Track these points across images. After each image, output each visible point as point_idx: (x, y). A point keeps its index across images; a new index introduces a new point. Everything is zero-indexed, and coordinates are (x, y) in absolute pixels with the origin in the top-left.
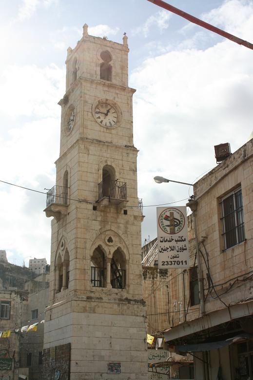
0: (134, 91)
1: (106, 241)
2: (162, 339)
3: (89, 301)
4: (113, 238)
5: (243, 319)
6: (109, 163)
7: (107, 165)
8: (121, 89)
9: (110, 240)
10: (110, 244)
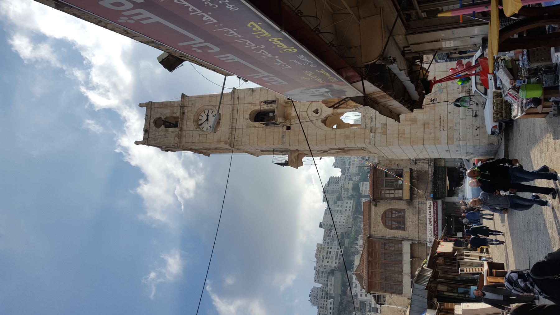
0: (183, 96)
1: (317, 115)
2: (461, 236)
3: (375, 130)
4: (314, 109)
5: (396, 98)
6: (248, 117)
7: (250, 119)
8: (183, 108)
9: (316, 112)
10: (319, 111)
